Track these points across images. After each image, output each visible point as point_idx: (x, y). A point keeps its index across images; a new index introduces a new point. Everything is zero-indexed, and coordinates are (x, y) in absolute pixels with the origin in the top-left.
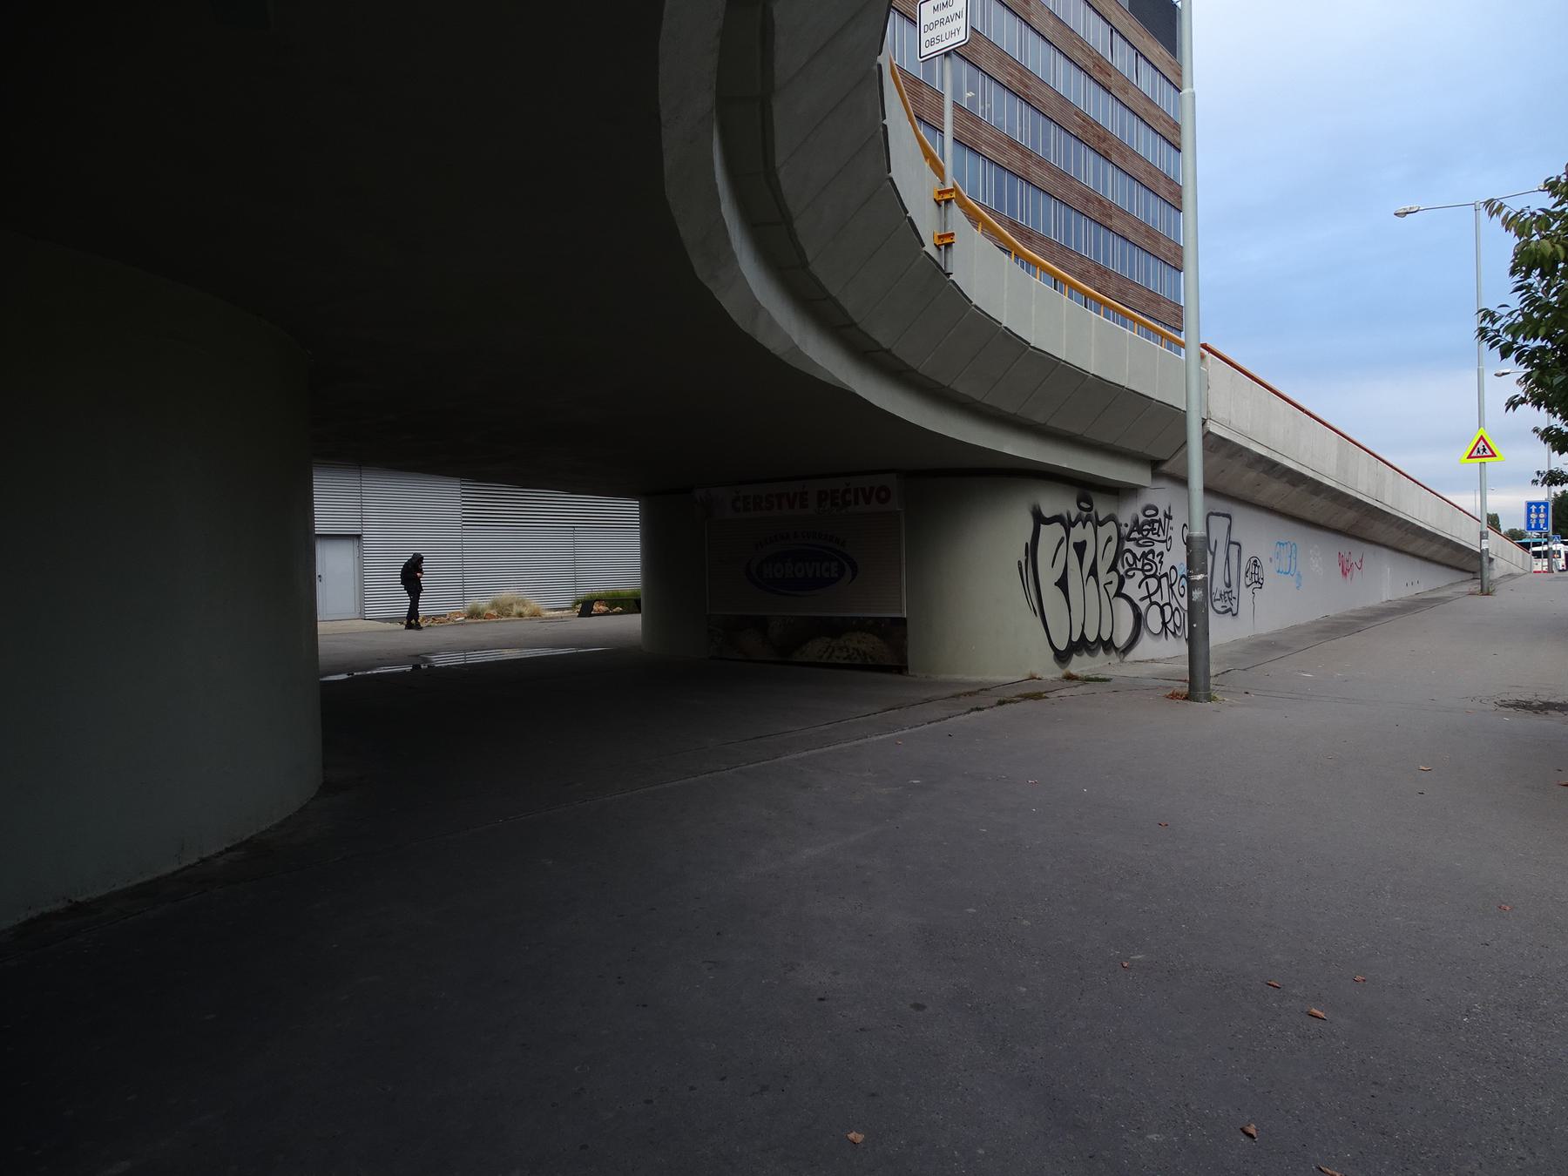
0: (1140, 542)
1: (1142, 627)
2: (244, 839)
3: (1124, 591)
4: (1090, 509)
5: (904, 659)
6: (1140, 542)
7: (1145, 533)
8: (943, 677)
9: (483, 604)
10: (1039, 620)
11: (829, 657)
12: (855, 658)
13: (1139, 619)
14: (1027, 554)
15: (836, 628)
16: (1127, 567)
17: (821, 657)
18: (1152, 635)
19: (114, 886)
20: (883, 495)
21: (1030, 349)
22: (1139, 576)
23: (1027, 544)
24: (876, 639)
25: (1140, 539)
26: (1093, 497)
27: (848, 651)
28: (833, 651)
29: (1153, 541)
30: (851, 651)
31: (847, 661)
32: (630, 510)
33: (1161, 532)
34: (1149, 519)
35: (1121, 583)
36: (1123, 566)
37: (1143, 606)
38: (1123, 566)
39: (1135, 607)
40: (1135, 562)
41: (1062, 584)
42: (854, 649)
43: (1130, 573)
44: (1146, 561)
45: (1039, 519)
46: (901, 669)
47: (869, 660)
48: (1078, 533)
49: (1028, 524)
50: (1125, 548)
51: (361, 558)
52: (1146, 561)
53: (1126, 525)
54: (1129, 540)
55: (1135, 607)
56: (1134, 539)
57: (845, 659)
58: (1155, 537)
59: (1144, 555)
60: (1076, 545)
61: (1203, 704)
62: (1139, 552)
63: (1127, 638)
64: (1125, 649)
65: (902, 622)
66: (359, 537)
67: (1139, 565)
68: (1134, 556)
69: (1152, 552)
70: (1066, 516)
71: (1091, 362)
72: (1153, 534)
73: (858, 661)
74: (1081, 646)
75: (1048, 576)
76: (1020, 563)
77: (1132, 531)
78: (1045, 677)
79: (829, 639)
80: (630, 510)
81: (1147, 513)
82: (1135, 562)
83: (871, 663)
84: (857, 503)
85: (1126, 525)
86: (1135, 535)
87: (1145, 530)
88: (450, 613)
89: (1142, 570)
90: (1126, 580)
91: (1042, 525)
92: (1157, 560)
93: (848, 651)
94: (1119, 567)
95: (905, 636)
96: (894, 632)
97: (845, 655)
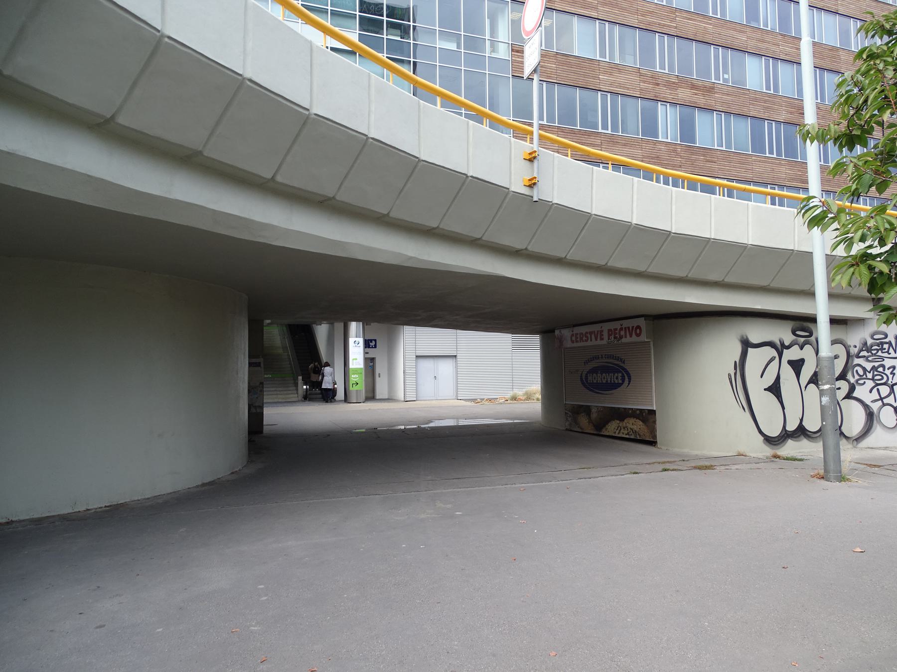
0: (870, 359)
1: (875, 422)
2: (119, 503)
3: (855, 394)
4: (811, 335)
5: (655, 437)
6: (870, 359)
7: (874, 352)
8: (677, 450)
9: (520, 393)
10: (747, 414)
11: (619, 433)
12: (631, 434)
13: (871, 416)
14: (735, 368)
15: (622, 415)
16: (857, 377)
17: (615, 433)
18: (891, 430)
19: (33, 515)
20: (638, 331)
21: (673, 234)
22: (870, 384)
23: (735, 362)
24: (641, 423)
25: (869, 356)
26: (812, 328)
27: (628, 430)
28: (621, 429)
29: (883, 359)
30: (629, 430)
31: (627, 436)
32: (536, 339)
33: (891, 351)
34: (878, 341)
35: (852, 388)
36: (854, 377)
37: (875, 407)
38: (854, 377)
39: (866, 406)
40: (865, 373)
41: (775, 389)
42: (631, 429)
43: (861, 382)
44: (876, 373)
45: (746, 344)
46: (653, 443)
47: (638, 436)
48: (793, 354)
49: (738, 349)
50: (855, 363)
51: (456, 367)
52: (876, 373)
53: (855, 347)
54: (858, 357)
55: (866, 406)
56: (864, 357)
57: (626, 434)
58: (886, 355)
59: (874, 369)
60: (790, 363)
61: (834, 484)
62: (869, 366)
63: (860, 430)
64: (858, 438)
65: (652, 412)
66: (455, 356)
67: (870, 376)
68: (864, 369)
69: (883, 366)
70: (779, 343)
71: (751, 237)
72: (883, 353)
73: (632, 437)
74: (786, 436)
75: (757, 386)
76: (729, 375)
77: (861, 350)
78: (751, 455)
79: (618, 422)
80: (536, 339)
81: (876, 337)
82: (865, 373)
83: (638, 438)
84: (626, 337)
85: (855, 347)
86: (864, 353)
87: (875, 350)
88: (500, 397)
89: (873, 379)
90: (857, 387)
91: (784, 350)
92: (888, 372)
93: (628, 430)
94: (849, 376)
95: (655, 422)
96: (648, 417)
97: (626, 432)
